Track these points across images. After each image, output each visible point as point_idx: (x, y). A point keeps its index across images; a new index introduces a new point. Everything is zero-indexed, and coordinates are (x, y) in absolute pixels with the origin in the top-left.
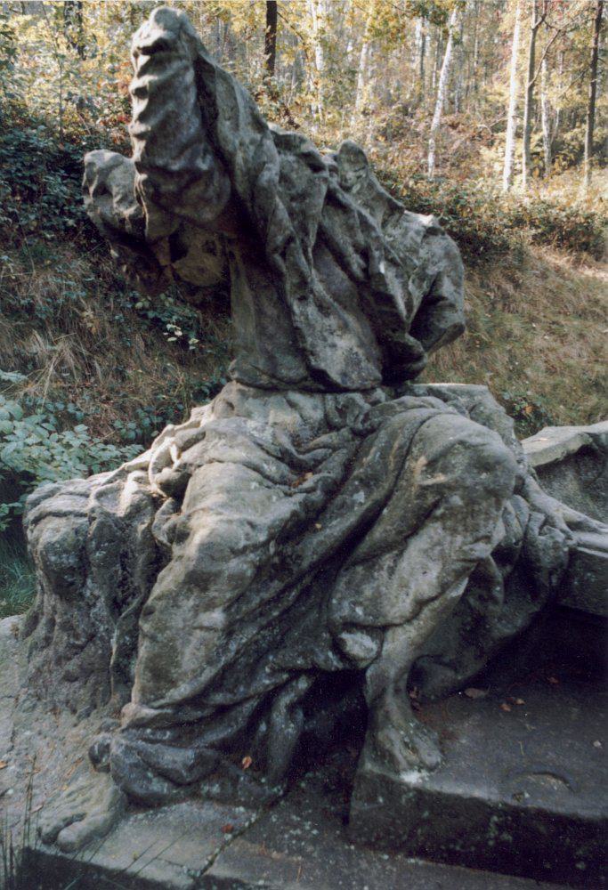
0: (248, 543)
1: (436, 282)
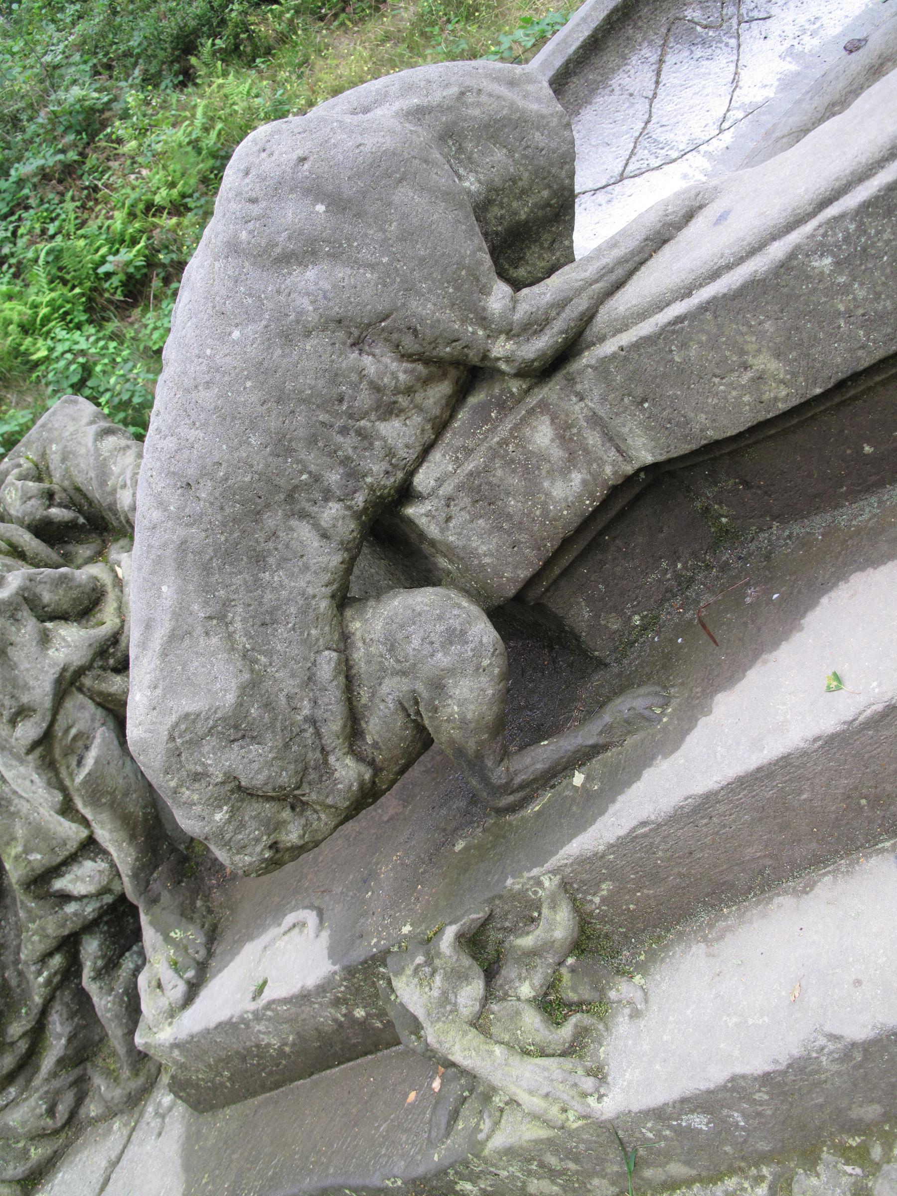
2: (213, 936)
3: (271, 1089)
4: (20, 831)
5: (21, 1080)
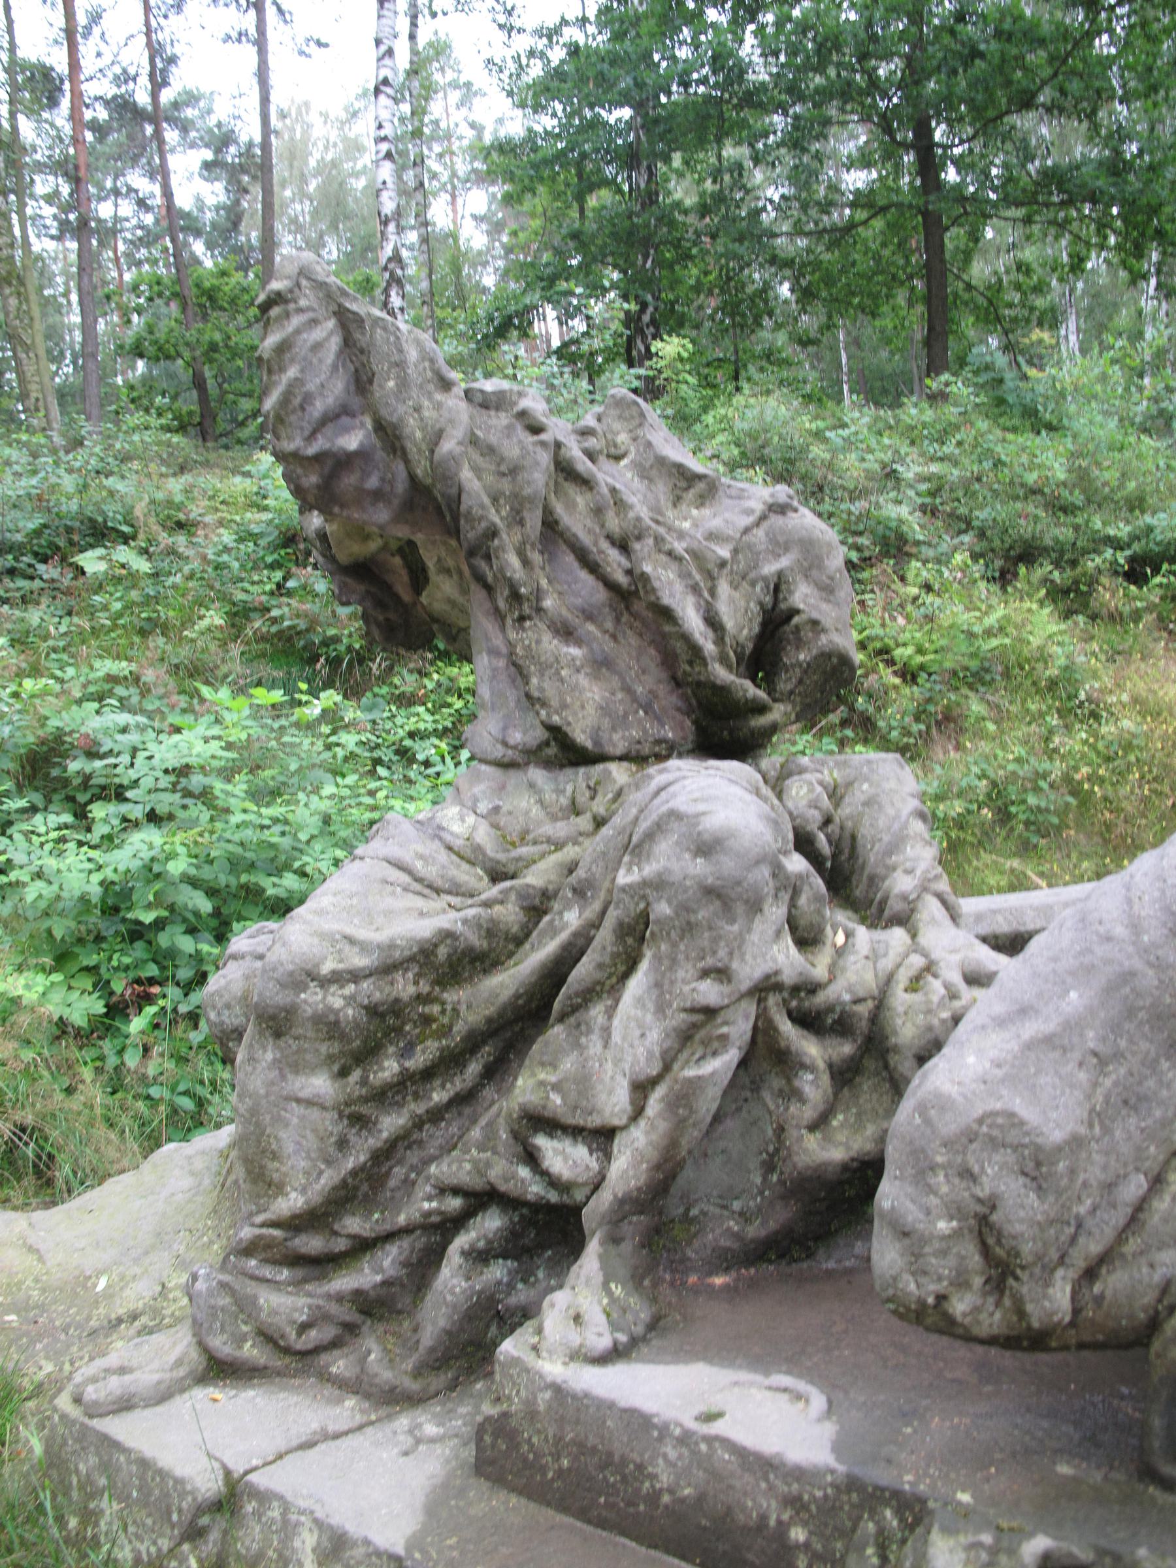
0: (341, 966)
1: (778, 586)
2: (654, 1325)
3: (589, 1522)
4: (568, 1064)
5: (300, 1273)
